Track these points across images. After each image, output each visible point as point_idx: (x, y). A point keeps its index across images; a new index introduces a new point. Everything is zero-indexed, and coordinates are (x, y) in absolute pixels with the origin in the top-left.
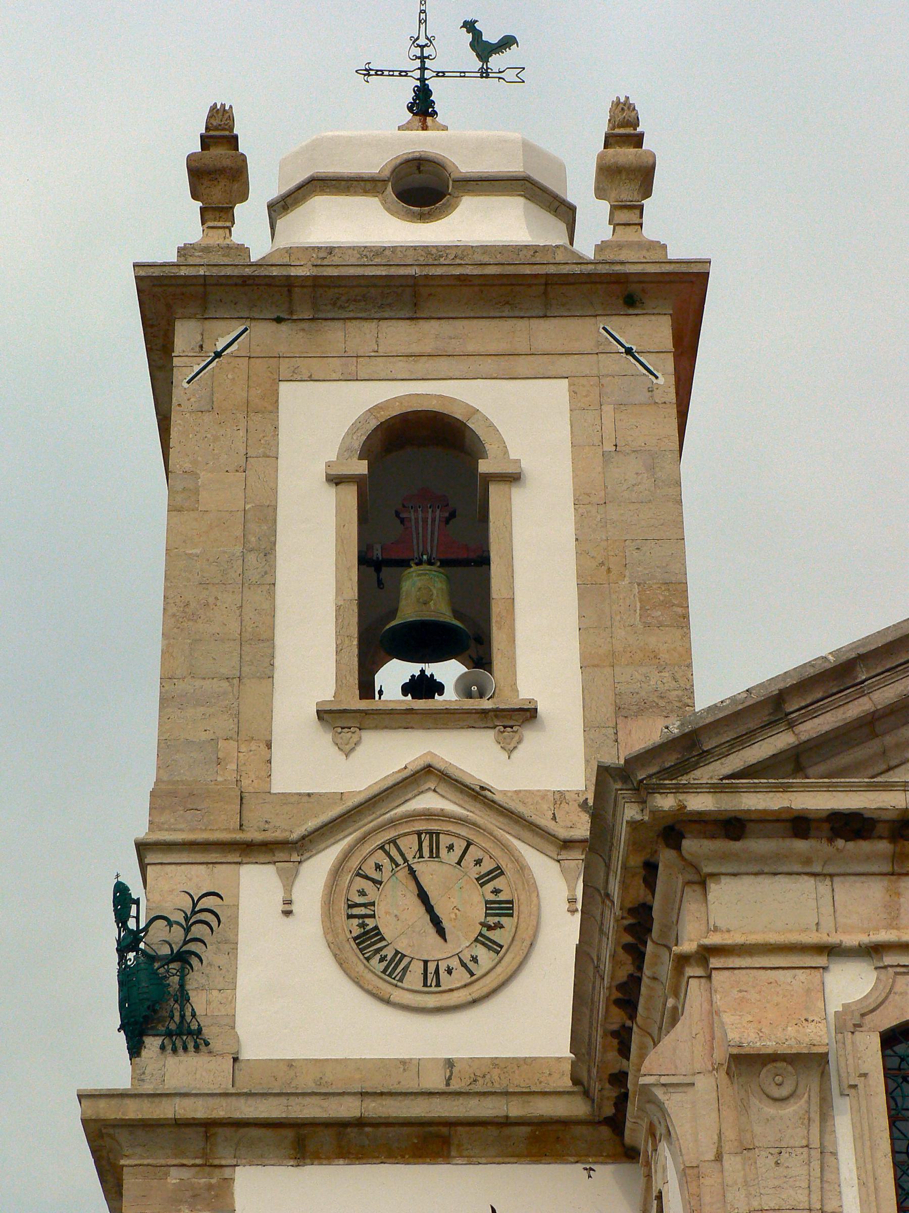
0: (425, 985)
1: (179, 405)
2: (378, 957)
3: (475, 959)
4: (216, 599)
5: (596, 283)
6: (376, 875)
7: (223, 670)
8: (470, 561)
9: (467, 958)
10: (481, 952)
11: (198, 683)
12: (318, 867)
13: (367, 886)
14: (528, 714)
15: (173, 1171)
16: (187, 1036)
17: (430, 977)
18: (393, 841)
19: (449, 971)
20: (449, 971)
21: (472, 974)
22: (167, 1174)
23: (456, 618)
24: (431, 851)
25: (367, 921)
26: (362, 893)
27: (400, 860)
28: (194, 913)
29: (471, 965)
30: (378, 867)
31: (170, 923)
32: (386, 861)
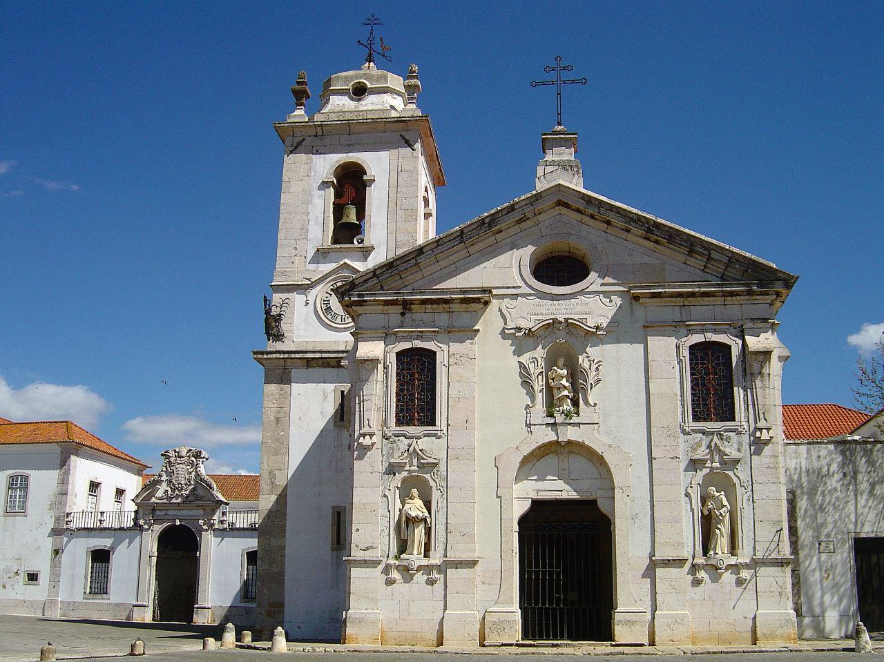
12: (313, 293)
16: (278, 337)
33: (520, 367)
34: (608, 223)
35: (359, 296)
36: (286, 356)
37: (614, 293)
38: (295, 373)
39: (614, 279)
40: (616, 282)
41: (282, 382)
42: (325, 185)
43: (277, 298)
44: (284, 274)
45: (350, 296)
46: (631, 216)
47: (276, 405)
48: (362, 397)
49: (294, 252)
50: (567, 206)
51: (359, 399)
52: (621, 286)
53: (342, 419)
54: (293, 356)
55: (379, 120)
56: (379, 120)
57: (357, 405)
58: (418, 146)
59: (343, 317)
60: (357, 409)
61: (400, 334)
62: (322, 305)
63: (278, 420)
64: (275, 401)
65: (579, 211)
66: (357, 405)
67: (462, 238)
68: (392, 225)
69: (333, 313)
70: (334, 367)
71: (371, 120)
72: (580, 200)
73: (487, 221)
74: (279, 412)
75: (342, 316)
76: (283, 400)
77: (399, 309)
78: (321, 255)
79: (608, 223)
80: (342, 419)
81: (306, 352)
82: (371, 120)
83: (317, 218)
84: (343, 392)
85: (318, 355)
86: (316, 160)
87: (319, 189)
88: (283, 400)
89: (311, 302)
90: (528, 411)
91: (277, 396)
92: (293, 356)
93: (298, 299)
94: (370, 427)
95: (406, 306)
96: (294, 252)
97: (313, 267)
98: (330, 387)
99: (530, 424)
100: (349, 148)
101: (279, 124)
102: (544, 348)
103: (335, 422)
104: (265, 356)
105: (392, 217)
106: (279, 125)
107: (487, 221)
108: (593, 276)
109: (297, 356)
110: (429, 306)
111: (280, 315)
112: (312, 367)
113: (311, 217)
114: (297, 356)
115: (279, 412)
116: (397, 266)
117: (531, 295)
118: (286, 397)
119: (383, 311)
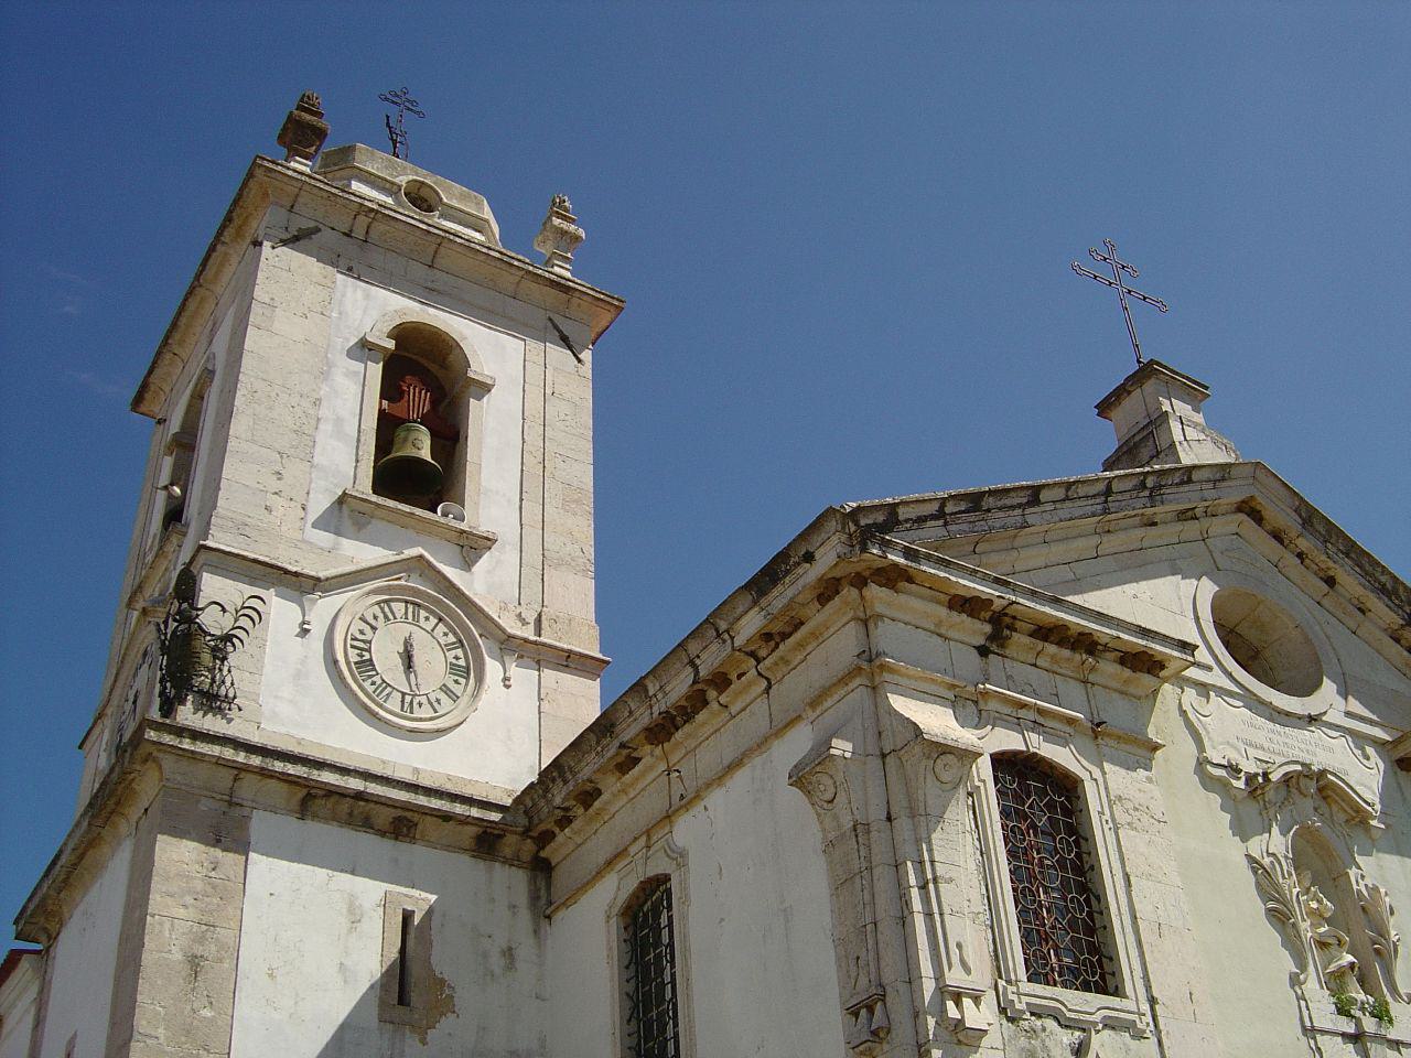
0: (402, 710)
1: (706, 808)
2: (370, 681)
3: (438, 701)
4: (277, 395)
5: (426, 814)
6: (373, 622)
7: (277, 446)
8: (450, 438)
9: (433, 698)
10: (443, 697)
11: (256, 448)
12: (323, 608)
13: (367, 629)
14: (486, 542)
15: (204, 800)
17: (406, 705)
18: (386, 601)
19: (420, 705)
20: (420, 705)
21: (436, 712)
22: (198, 802)
23: (433, 459)
24: (414, 616)
25: (364, 653)
26: (362, 632)
27: (391, 617)
28: (243, 608)
29: (435, 704)
30: (375, 618)
31: (224, 610)
32: (381, 616)
33: (1255, 872)
34: (1330, 582)
35: (909, 554)
36: (256, 761)
37: (1375, 742)
38: (261, 824)
39: (1366, 706)
40: (1375, 718)
41: (216, 842)
42: (365, 348)
43: (212, 586)
44: (241, 529)
45: (885, 544)
46: (1383, 579)
47: (191, 913)
48: (928, 865)
49: (275, 485)
50: (1257, 517)
51: (921, 872)
52: (1386, 732)
53: (403, 1000)
54: (278, 766)
55: (516, 263)
56: (516, 263)
57: (915, 892)
58: (586, 355)
59: (408, 699)
60: (917, 905)
61: (993, 705)
62: (350, 650)
63: (195, 964)
64: (189, 900)
65: (1277, 536)
66: (915, 892)
67: (1106, 502)
68: (532, 509)
69: (377, 679)
70: (382, 834)
71: (497, 255)
72: (1289, 511)
73: (1150, 482)
74: (201, 939)
75: (404, 694)
76: (216, 900)
77: (978, 630)
78: (345, 514)
79: (1330, 582)
80: (403, 1000)
81: (321, 765)
82: (497, 255)
83: (339, 421)
84: (407, 917)
85: (355, 784)
86: (345, 286)
87: (350, 354)
88: (216, 900)
89: (318, 630)
90: (1299, 992)
91: (199, 885)
92: (278, 766)
93: (280, 610)
94: (967, 970)
95: (1001, 624)
96: (275, 485)
97: (324, 538)
98: (370, 891)
99: (1313, 1027)
100: (430, 294)
101: (273, 162)
102: (1284, 833)
103: (383, 1004)
104: (186, 744)
105: (533, 486)
106: (270, 165)
107: (1150, 482)
108: (1328, 686)
109: (291, 769)
110: (1052, 649)
111: (228, 638)
112: (315, 817)
113: (324, 412)
114: (291, 769)
115: (201, 939)
116: (989, 510)
117: (1231, 694)
118: (233, 893)
119: (939, 624)
